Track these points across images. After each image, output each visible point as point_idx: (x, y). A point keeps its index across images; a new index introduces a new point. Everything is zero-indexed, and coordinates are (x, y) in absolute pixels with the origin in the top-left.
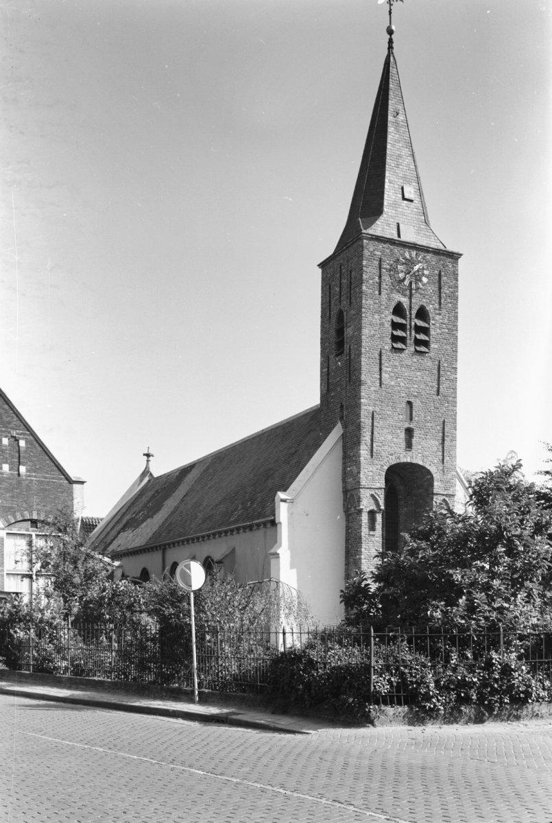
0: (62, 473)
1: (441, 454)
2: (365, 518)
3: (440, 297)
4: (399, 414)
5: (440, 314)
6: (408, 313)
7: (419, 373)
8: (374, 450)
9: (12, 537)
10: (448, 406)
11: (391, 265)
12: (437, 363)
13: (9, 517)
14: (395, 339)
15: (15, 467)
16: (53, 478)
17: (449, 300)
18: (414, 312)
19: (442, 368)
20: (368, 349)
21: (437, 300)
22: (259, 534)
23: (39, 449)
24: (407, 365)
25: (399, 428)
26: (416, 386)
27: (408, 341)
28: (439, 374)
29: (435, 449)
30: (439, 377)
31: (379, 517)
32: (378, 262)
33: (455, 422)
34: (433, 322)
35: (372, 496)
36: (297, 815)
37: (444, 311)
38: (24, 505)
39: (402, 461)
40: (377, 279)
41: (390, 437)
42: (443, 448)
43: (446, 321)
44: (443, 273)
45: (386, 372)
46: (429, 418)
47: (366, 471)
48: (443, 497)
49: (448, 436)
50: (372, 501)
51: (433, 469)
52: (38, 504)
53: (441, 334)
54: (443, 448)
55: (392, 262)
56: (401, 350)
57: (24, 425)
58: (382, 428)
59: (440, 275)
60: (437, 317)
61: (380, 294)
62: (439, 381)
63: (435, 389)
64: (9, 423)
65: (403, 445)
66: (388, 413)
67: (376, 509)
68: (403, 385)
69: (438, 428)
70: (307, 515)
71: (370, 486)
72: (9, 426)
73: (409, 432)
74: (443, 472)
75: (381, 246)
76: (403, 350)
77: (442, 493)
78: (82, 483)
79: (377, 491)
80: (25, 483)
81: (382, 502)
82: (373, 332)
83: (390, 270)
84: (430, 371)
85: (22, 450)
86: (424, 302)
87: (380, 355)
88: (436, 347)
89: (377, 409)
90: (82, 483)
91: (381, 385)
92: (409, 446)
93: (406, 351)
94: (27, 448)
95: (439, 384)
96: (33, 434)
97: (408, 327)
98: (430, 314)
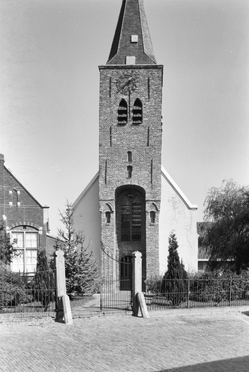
0: (38, 204)
1: (150, 178)
2: (104, 216)
3: (149, 92)
4: (123, 159)
5: (149, 101)
6: (128, 104)
7: (135, 135)
8: (107, 180)
9: (30, 233)
10: (155, 151)
11: (118, 80)
12: (147, 128)
13: (12, 225)
14: (120, 119)
15: (15, 203)
16: (34, 207)
17: (155, 92)
18: (132, 103)
19: (150, 131)
20: (103, 127)
21: (147, 94)
23: (27, 194)
24: (127, 132)
25: (123, 167)
26: (133, 143)
27: (128, 119)
28: (148, 134)
29: (146, 176)
30: (148, 136)
31: (113, 216)
32: (109, 80)
33: (160, 160)
34: (145, 106)
35: (107, 204)
37: (152, 99)
38: (20, 219)
39: (125, 184)
40: (108, 89)
41: (117, 172)
42: (152, 175)
43: (153, 104)
44: (151, 78)
45: (114, 138)
46: (142, 159)
47: (102, 191)
48: (152, 202)
49: (155, 168)
50: (108, 207)
51: (145, 187)
52: (26, 218)
53: (150, 112)
54: (152, 175)
55: (118, 79)
56: (124, 125)
57: (20, 184)
58: (112, 167)
59: (149, 80)
60: (147, 103)
61: (110, 97)
62: (148, 138)
63: (146, 143)
64: (12, 184)
65: (127, 176)
66: (116, 159)
67: (110, 211)
68: (125, 143)
69: (149, 164)
70: (81, 216)
71: (104, 199)
72: (12, 185)
73: (130, 168)
74: (152, 188)
75: (111, 71)
76: (125, 124)
77: (151, 199)
78: (48, 208)
79: (109, 202)
80: (19, 210)
82: (106, 118)
83: (117, 83)
84: (143, 133)
85: (18, 195)
86: (138, 96)
87: (111, 129)
88: (147, 119)
89: (109, 158)
90: (48, 208)
91: (111, 145)
92: (130, 175)
93: (127, 125)
94: (21, 194)
95: (148, 140)
96: (23, 188)
97: (128, 111)
98: (143, 102)
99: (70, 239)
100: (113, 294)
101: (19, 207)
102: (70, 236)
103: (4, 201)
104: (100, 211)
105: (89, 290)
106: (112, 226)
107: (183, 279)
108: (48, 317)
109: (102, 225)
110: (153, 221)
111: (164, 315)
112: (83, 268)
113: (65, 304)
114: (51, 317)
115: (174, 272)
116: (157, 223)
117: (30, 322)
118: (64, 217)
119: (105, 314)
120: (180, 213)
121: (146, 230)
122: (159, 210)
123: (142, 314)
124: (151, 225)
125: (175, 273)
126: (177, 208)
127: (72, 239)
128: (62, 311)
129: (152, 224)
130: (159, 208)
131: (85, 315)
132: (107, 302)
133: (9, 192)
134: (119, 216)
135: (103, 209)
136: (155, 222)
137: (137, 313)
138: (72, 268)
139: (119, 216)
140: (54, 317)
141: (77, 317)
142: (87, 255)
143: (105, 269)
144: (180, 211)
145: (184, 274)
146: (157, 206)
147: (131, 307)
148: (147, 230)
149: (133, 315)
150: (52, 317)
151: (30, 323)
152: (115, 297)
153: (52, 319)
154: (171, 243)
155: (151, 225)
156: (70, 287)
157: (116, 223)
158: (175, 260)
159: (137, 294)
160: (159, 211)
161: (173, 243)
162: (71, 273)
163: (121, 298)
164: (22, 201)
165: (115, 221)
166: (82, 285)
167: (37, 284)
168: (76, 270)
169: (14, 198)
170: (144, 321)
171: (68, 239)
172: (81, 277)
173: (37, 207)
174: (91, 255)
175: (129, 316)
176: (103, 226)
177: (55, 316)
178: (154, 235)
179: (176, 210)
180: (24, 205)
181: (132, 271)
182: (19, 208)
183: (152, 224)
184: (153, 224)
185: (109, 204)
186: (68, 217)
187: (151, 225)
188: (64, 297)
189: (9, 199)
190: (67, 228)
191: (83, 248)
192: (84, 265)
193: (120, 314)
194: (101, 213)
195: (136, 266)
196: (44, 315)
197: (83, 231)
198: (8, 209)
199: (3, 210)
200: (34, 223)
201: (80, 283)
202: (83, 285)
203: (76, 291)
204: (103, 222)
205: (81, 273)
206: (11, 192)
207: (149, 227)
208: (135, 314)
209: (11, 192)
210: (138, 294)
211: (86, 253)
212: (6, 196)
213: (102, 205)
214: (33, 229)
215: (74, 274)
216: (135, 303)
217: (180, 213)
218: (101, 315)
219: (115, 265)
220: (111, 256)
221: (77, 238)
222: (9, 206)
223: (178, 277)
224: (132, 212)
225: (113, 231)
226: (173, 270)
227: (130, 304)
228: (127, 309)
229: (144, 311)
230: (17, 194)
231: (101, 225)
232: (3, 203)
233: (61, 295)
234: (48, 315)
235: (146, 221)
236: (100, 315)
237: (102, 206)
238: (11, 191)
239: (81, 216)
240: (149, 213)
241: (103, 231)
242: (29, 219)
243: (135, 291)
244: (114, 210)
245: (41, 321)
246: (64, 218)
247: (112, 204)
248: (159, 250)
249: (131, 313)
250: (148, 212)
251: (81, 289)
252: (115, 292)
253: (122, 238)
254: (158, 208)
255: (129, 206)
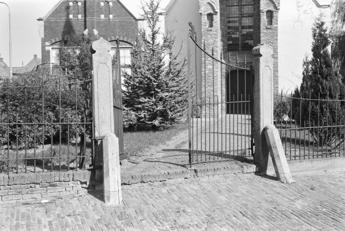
2: (205, 19)
16: (127, 19)
23: (120, 5)
31: (217, 18)
38: (112, 34)
67: (212, 12)
70: (177, 21)
94: (113, 6)
99: (153, 42)
100: (216, 119)
101: (112, 20)
102: (153, 38)
103: (95, 14)
104: (200, 12)
105: (180, 116)
106: (216, 31)
107: (340, 99)
108: (71, 184)
109: (203, 30)
110: (270, 22)
111: (318, 169)
112: (171, 83)
113: (107, 155)
114: (79, 182)
115: (323, 88)
116: (275, 26)
117: (30, 196)
118: (146, 12)
119: (198, 174)
120: (305, 13)
121: (261, 36)
122: (278, 8)
123: (277, 172)
124: (267, 28)
125: (326, 88)
126: (302, 6)
127: (157, 41)
128: (101, 168)
129: (269, 27)
130: (279, 6)
131: (154, 176)
132: (208, 135)
133: (100, 4)
134: (224, 20)
135: (203, 10)
136: (273, 24)
137: (265, 169)
138: (155, 84)
139: (224, 20)
140: (86, 183)
141: (137, 181)
142: (178, 64)
143: (206, 86)
144: (305, 10)
145: (340, 90)
146: (276, 3)
147: (253, 155)
148: (262, 34)
149: (257, 173)
150: (82, 183)
151: (27, 198)
152: (220, 126)
153: (80, 186)
154: (316, 38)
155: (267, 28)
156: (153, 111)
157: (221, 28)
158: (324, 66)
159: (265, 129)
160: (279, 9)
161: (320, 37)
162: (154, 90)
163: (228, 127)
164: (114, 13)
165: (220, 26)
166: (170, 109)
167: (88, 109)
168: (162, 86)
169: (106, 11)
170: (282, 191)
171: (152, 42)
172: (168, 97)
173: (131, 19)
174: (184, 64)
175: (249, 175)
176: (204, 32)
177: (88, 180)
178: (271, 41)
179: (301, 8)
180: (117, 18)
181: (253, 83)
182: (112, 22)
183: (269, 27)
184: (270, 27)
185: (211, 3)
186: (151, 11)
187: (267, 28)
188: (107, 140)
189: (100, 12)
190: (150, 27)
191: (171, 54)
192: (174, 80)
193: (229, 172)
194: (201, 15)
195: (261, 72)
196: (62, 179)
197: (173, 31)
198: (99, 23)
199: (94, 24)
200: (128, 37)
201: (166, 105)
202: (172, 109)
203: (160, 117)
204: (203, 27)
205: (168, 91)
206: (102, 4)
207: (265, 31)
208: (261, 172)
209: (102, 4)
210: (268, 131)
211: (177, 61)
212: (97, 8)
213: (203, 4)
214: (127, 44)
215: (157, 92)
216: (260, 148)
217: (305, 13)
218: (190, 174)
219: (220, 81)
220: (211, 54)
221: (165, 41)
222: (100, 19)
223: (331, 96)
224: (240, 14)
225: (216, 38)
226: (322, 84)
227: (249, 149)
228: (241, 159)
229: (281, 166)
230: (109, 5)
231: (201, 31)
232: (94, 17)
233: (102, 135)
234: (71, 178)
235: (260, 24)
236: (188, 176)
237: (202, 6)
238: (103, 3)
239: (177, 21)
240: (265, 13)
241: (204, 38)
242: (122, 33)
243: (261, 124)
244: (218, 10)
245: (52, 192)
246: (146, 13)
247: (215, 3)
248: (278, 61)
249: (253, 168)
250: (264, 11)
251: (168, 115)
252: (220, 116)
253: (228, 48)
254: (277, 5)
255: (238, 7)
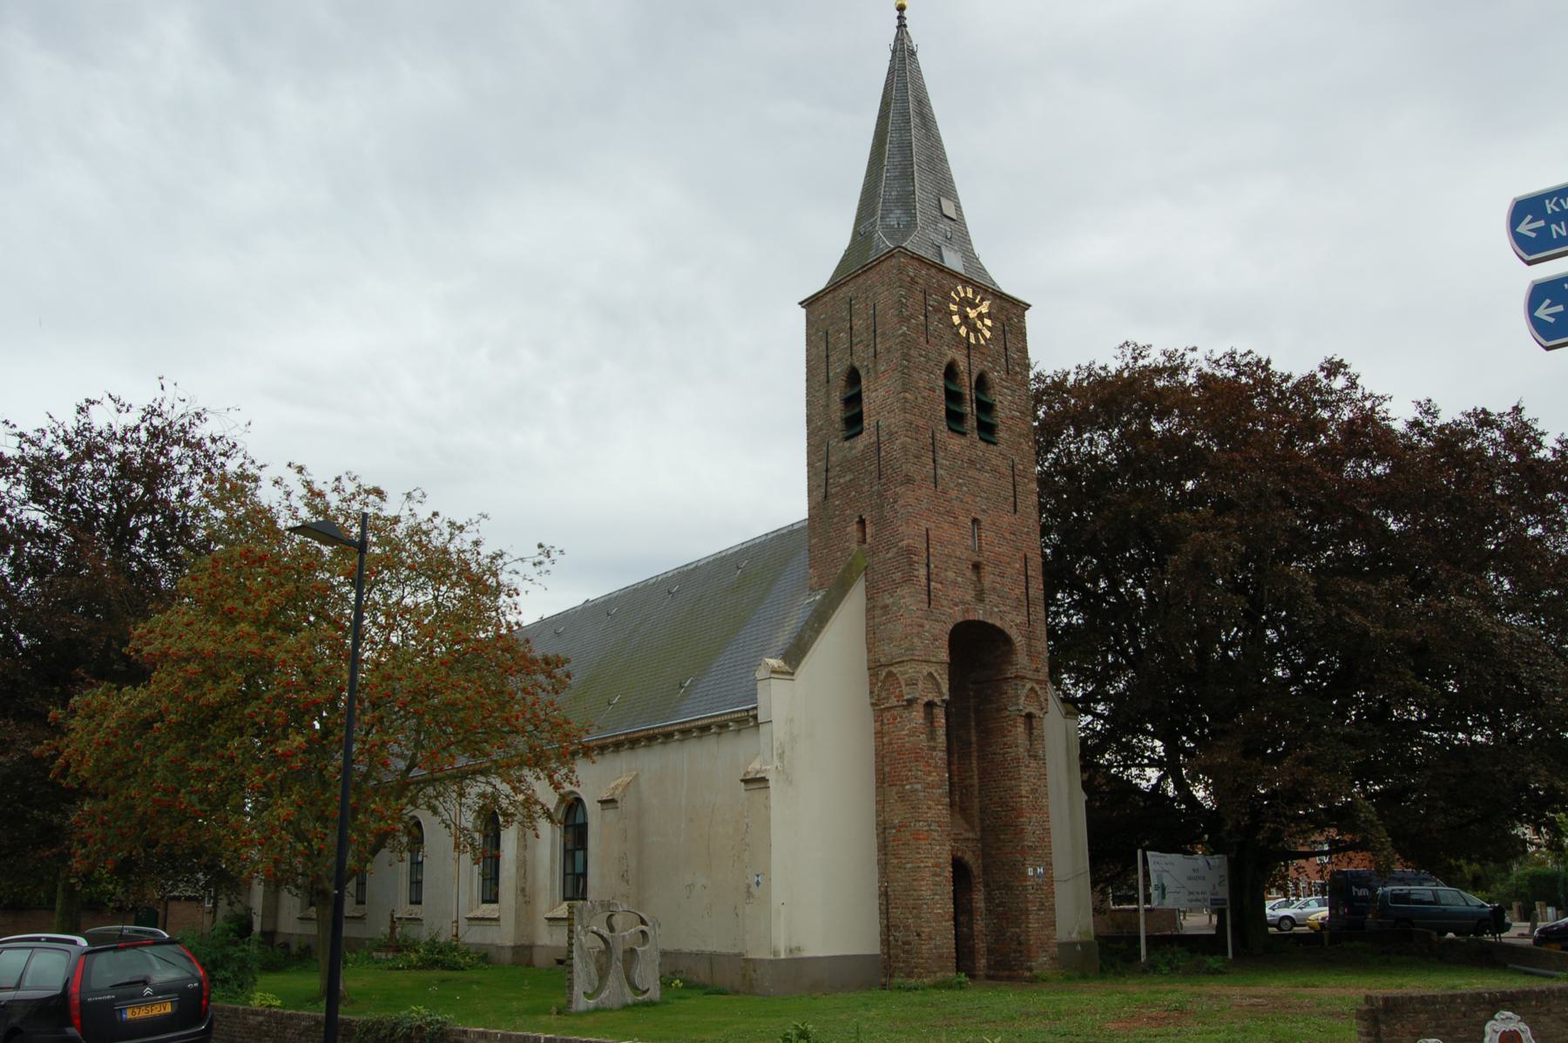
22: (519, 943)
31: (940, 714)
36: (1191, 901)
51: (1014, 634)
81: (945, 688)
